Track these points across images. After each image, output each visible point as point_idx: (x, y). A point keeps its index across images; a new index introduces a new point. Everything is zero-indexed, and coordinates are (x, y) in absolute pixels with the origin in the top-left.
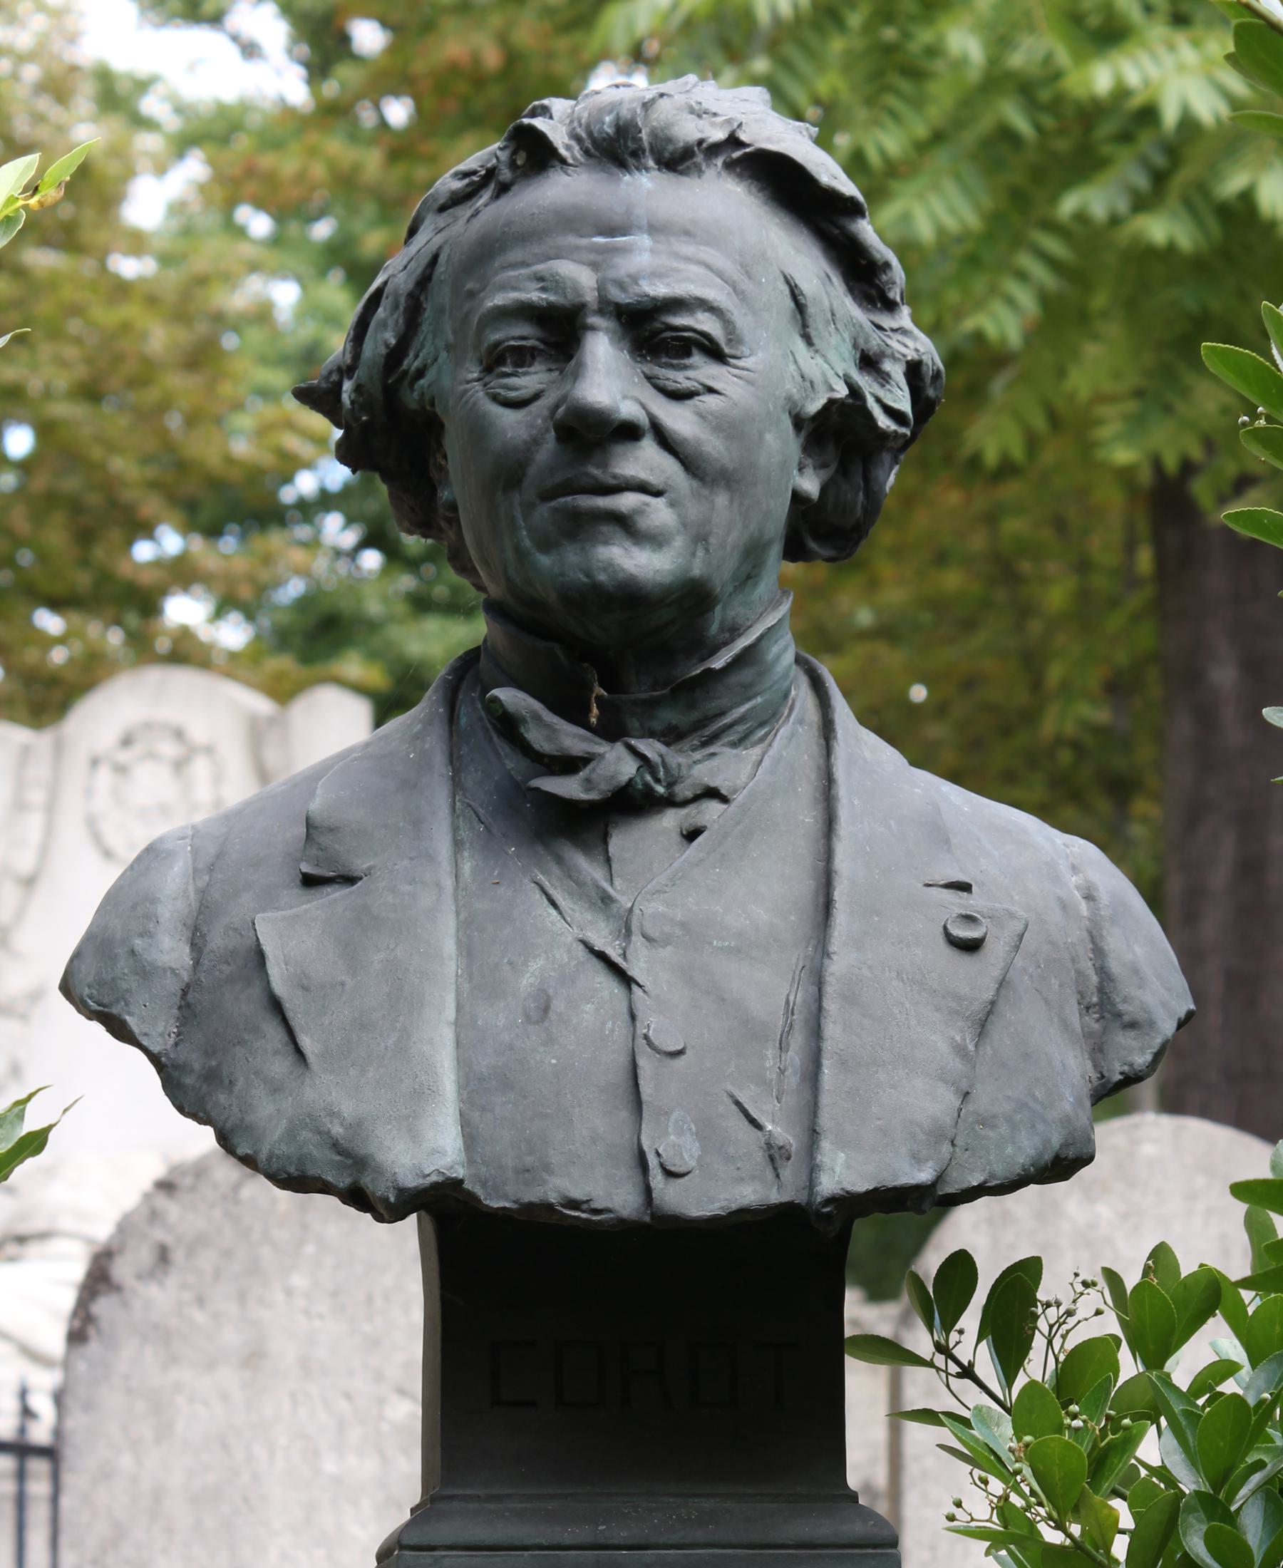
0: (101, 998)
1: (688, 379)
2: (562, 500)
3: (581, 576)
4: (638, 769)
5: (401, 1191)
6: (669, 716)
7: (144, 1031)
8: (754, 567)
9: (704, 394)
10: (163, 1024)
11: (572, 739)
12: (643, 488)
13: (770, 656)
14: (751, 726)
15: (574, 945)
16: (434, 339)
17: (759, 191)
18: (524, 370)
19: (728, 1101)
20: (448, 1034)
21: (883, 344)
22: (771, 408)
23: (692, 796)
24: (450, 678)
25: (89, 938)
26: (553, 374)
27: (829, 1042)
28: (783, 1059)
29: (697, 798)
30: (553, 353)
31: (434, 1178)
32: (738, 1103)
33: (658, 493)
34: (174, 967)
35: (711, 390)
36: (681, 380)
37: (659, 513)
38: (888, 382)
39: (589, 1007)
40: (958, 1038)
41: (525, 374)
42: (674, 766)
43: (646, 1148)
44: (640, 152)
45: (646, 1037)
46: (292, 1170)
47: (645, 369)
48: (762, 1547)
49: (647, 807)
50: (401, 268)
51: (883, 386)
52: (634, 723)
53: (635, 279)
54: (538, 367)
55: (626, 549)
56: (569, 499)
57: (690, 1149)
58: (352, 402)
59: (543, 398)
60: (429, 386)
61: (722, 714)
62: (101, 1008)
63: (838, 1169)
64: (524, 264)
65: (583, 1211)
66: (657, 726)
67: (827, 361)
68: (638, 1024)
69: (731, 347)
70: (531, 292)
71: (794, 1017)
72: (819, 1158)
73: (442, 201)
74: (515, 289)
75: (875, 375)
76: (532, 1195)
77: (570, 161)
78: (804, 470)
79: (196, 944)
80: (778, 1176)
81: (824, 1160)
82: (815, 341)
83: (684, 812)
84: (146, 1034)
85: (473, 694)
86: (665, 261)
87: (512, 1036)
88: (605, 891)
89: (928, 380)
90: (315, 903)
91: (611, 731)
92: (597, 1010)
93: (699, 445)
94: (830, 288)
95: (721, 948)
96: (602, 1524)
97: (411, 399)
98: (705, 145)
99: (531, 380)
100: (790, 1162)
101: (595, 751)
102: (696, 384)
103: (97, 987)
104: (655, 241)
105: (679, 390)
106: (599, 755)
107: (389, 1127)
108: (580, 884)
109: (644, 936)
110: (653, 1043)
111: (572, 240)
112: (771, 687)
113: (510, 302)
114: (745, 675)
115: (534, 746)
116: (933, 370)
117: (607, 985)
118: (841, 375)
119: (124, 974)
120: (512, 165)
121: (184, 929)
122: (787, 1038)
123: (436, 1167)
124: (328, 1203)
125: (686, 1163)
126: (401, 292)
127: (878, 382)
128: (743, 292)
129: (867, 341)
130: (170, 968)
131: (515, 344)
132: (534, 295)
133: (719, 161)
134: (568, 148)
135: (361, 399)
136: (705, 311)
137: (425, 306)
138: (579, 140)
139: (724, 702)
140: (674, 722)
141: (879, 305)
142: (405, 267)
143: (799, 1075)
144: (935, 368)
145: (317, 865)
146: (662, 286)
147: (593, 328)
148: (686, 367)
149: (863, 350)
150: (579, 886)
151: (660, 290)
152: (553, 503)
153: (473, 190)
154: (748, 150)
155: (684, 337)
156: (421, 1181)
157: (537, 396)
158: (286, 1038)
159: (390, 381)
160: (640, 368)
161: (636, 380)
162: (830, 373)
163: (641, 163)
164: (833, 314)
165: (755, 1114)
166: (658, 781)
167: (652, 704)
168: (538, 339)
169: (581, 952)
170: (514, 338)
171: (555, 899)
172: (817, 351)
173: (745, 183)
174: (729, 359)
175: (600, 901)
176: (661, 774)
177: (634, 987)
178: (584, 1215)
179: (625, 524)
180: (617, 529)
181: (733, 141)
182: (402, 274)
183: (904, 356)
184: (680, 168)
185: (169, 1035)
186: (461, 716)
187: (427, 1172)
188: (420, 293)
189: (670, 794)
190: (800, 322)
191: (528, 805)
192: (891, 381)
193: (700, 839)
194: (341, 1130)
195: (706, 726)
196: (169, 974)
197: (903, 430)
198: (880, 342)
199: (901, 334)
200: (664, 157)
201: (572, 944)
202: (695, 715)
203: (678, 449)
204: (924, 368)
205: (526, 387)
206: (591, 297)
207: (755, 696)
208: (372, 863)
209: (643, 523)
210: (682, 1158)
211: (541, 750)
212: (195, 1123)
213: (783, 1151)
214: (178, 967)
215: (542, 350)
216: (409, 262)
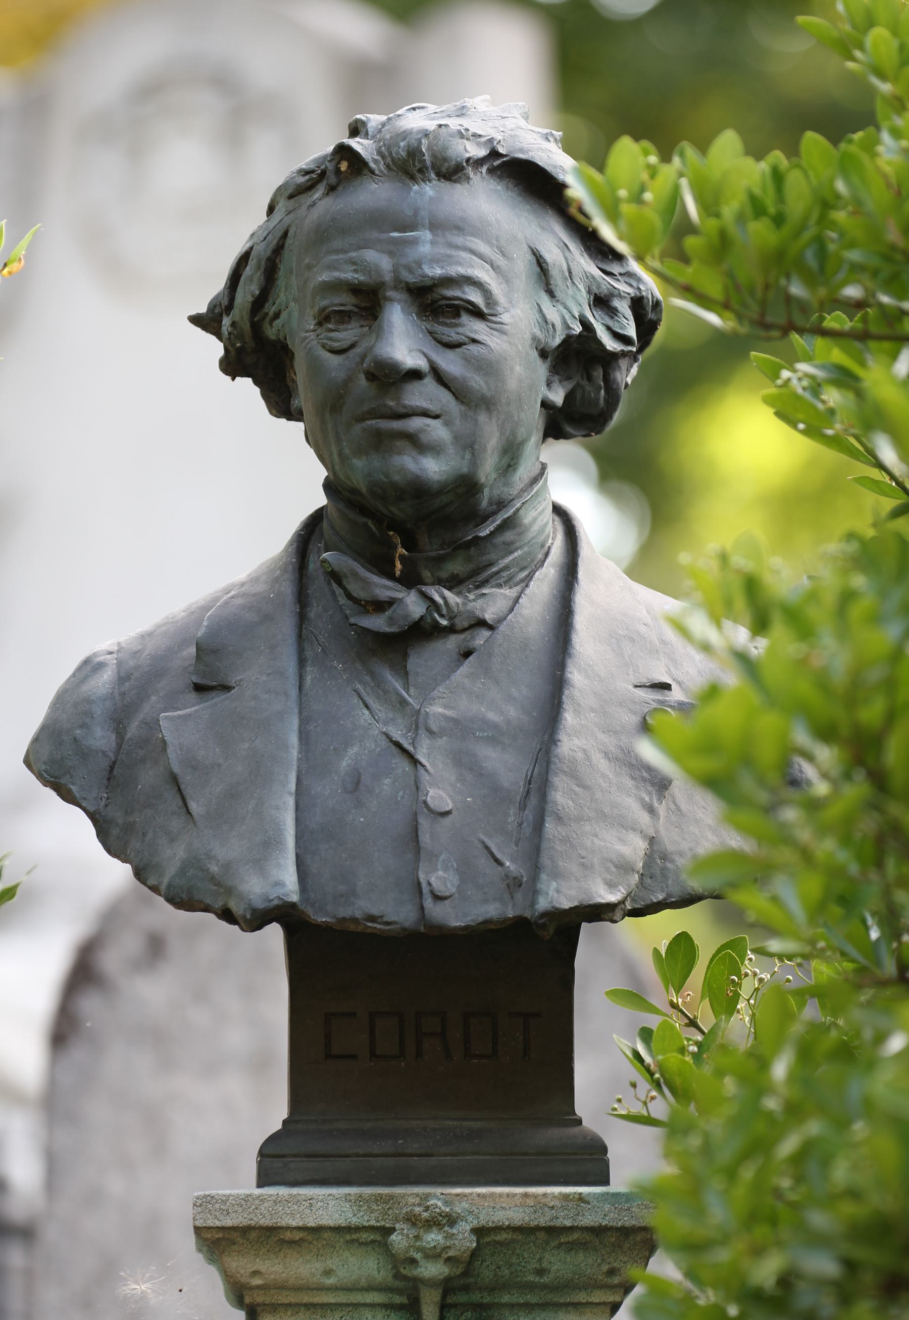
0: (53, 772)
1: (458, 333)
2: (369, 422)
3: (382, 477)
4: (427, 608)
5: (254, 911)
6: (456, 567)
7: (83, 796)
8: (512, 459)
9: (469, 343)
10: (97, 791)
11: (383, 588)
12: (425, 414)
13: (526, 521)
14: (513, 572)
15: (380, 736)
16: (285, 292)
17: (515, 186)
18: (345, 326)
19: (480, 846)
20: (291, 802)
21: (612, 287)
22: (521, 348)
23: (467, 625)
24: (302, 533)
25: (44, 728)
26: (364, 329)
27: (550, 805)
28: (521, 815)
29: (471, 627)
30: (364, 314)
31: (276, 902)
32: (487, 848)
33: (436, 417)
34: (104, 750)
35: (474, 341)
36: (452, 335)
37: (437, 431)
38: (616, 315)
39: (387, 781)
40: (647, 799)
41: (346, 330)
42: (454, 605)
43: (421, 880)
44: (424, 169)
45: (425, 802)
46: (184, 896)
47: (428, 327)
48: (511, 1154)
49: (436, 634)
50: (262, 239)
51: (612, 318)
52: (426, 574)
53: (419, 264)
54: (354, 324)
55: (413, 457)
56: (374, 422)
57: (452, 880)
58: (230, 333)
59: (357, 347)
60: (283, 325)
61: (491, 564)
62: (53, 779)
63: (551, 893)
64: (343, 251)
65: (379, 923)
66: (444, 575)
67: (566, 307)
68: (420, 793)
69: (490, 309)
70: (347, 272)
71: (531, 786)
72: (539, 886)
73: (290, 191)
74: (336, 269)
75: (606, 310)
76: (345, 912)
77: (377, 172)
78: (552, 385)
79: (120, 733)
80: (512, 898)
81: (542, 887)
82: (556, 294)
83: (462, 636)
84: (84, 799)
85: (319, 545)
86: (443, 250)
87: (334, 802)
88: (402, 697)
89: (649, 309)
90: (202, 705)
91: (410, 580)
92: (393, 783)
93: (465, 381)
94: (567, 254)
95: (482, 737)
96: (401, 1139)
97: (271, 332)
98: (471, 161)
99: (346, 335)
100: (521, 888)
101: (396, 597)
102: (463, 337)
103: (50, 764)
104: (434, 235)
105: (451, 342)
106: (399, 599)
107: (248, 867)
108: (386, 692)
109: (427, 730)
110: (429, 807)
111: (375, 234)
112: (529, 542)
113: (333, 279)
114: (508, 536)
115: (353, 594)
116: (653, 301)
117: (404, 765)
118: (577, 317)
119: (69, 755)
120: (338, 171)
121: (112, 721)
122: (525, 801)
123: (277, 895)
124: (210, 917)
125: (449, 890)
126: (262, 257)
127: (609, 316)
128: (498, 267)
129: (599, 287)
130: (101, 751)
131: (336, 309)
132: (348, 275)
133: (484, 169)
134: (375, 161)
135: (235, 332)
136: (469, 285)
137: (279, 266)
138: (383, 157)
139: (493, 556)
140: (455, 572)
141: (610, 257)
142: (265, 239)
143: (531, 828)
144: (655, 300)
145: (204, 677)
146: (438, 269)
147: (390, 300)
148: (456, 325)
149: (596, 294)
150: (384, 693)
151: (438, 271)
152: (363, 425)
153: (313, 184)
154: (505, 159)
155: (455, 304)
156: (267, 904)
157: (352, 346)
158: (181, 803)
159: (256, 319)
160: (425, 326)
161: (421, 336)
162: (568, 317)
163: (425, 176)
164: (570, 272)
165: (499, 856)
166: (442, 616)
167: (440, 560)
168: (353, 305)
169: (384, 743)
170: (336, 305)
171: (367, 703)
172: (558, 301)
173: (504, 182)
174: (490, 317)
175: (398, 705)
176: (444, 611)
177: (418, 765)
178: (379, 926)
179: (414, 441)
180: (407, 443)
181: (494, 154)
182: (263, 243)
183: (629, 294)
184: (454, 178)
185: (101, 799)
186: (310, 563)
187: (271, 898)
188: (276, 257)
189: (452, 624)
190: (544, 281)
191: (352, 633)
192: (618, 314)
193: (471, 658)
194: (216, 869)
195: (479, 574)
196: (100, 755)
197: (630, 348)
198: (609, 286)
199: (628, 276)
200: (442, 172)
201: (377, 736)
202: (471, 567)
203: (450, 385)
204: (646, 301)
205: (345, 340)
206: (388, 277)
207: (516, 550)
208: (241, 677)
209: (424, 438)
210: (446, 886)
211: (358, 597)
212: (119, 862)
213: (517, 880)
214: (107, 750)
215: (356, 313)
216: (268, 235)
